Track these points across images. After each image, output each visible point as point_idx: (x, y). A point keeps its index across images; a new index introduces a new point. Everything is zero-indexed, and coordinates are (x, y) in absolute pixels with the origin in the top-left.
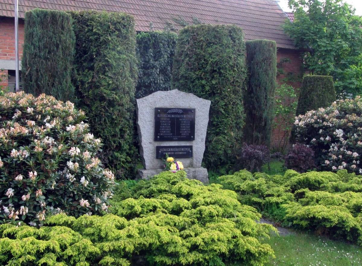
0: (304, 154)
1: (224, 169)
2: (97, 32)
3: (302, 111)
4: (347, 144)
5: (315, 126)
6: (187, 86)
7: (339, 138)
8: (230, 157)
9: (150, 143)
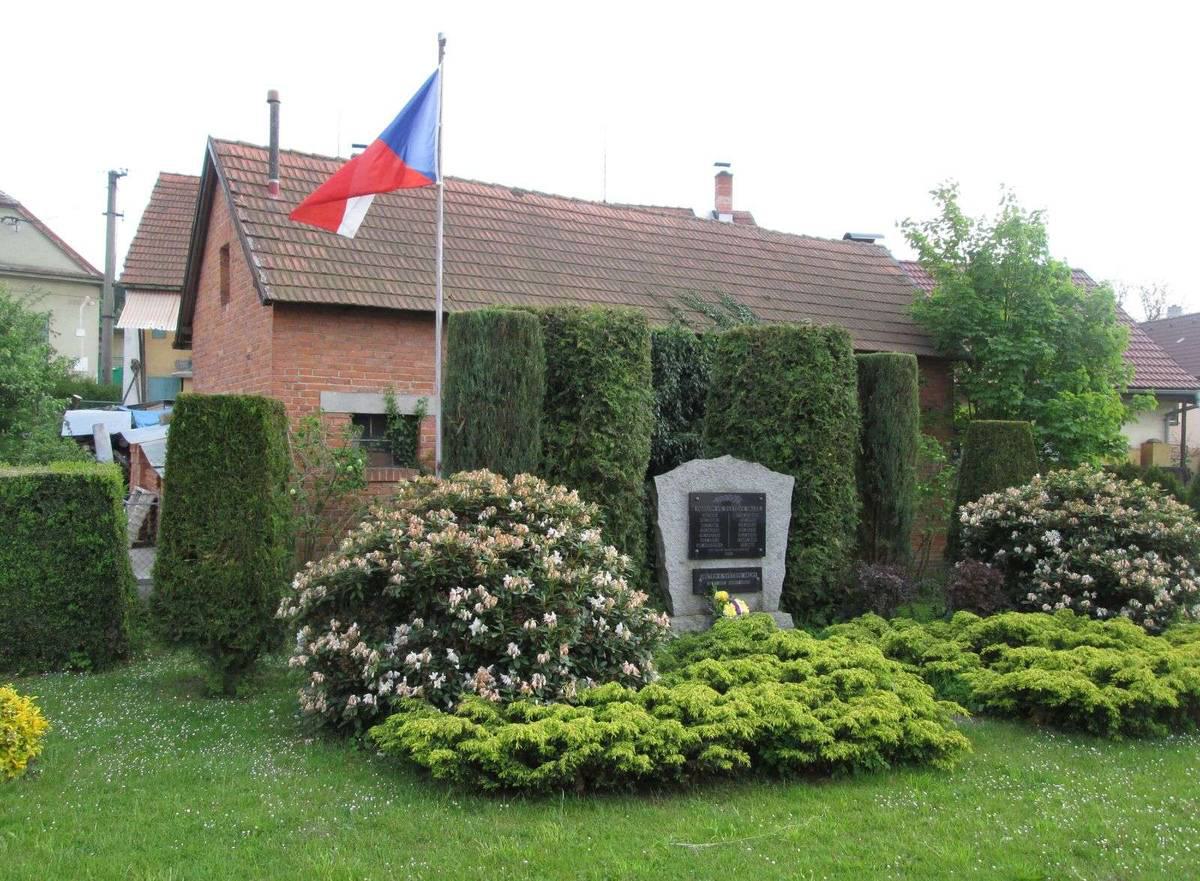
0: (986, 581)
1: (821, 614)
2: (585, 347)
3: (970, 491)
4: (1070, 559)
5: (1003, 524)
6: (741, 446)
7: (1051, 547)
8: (832, 591)
9: (681, 563)
